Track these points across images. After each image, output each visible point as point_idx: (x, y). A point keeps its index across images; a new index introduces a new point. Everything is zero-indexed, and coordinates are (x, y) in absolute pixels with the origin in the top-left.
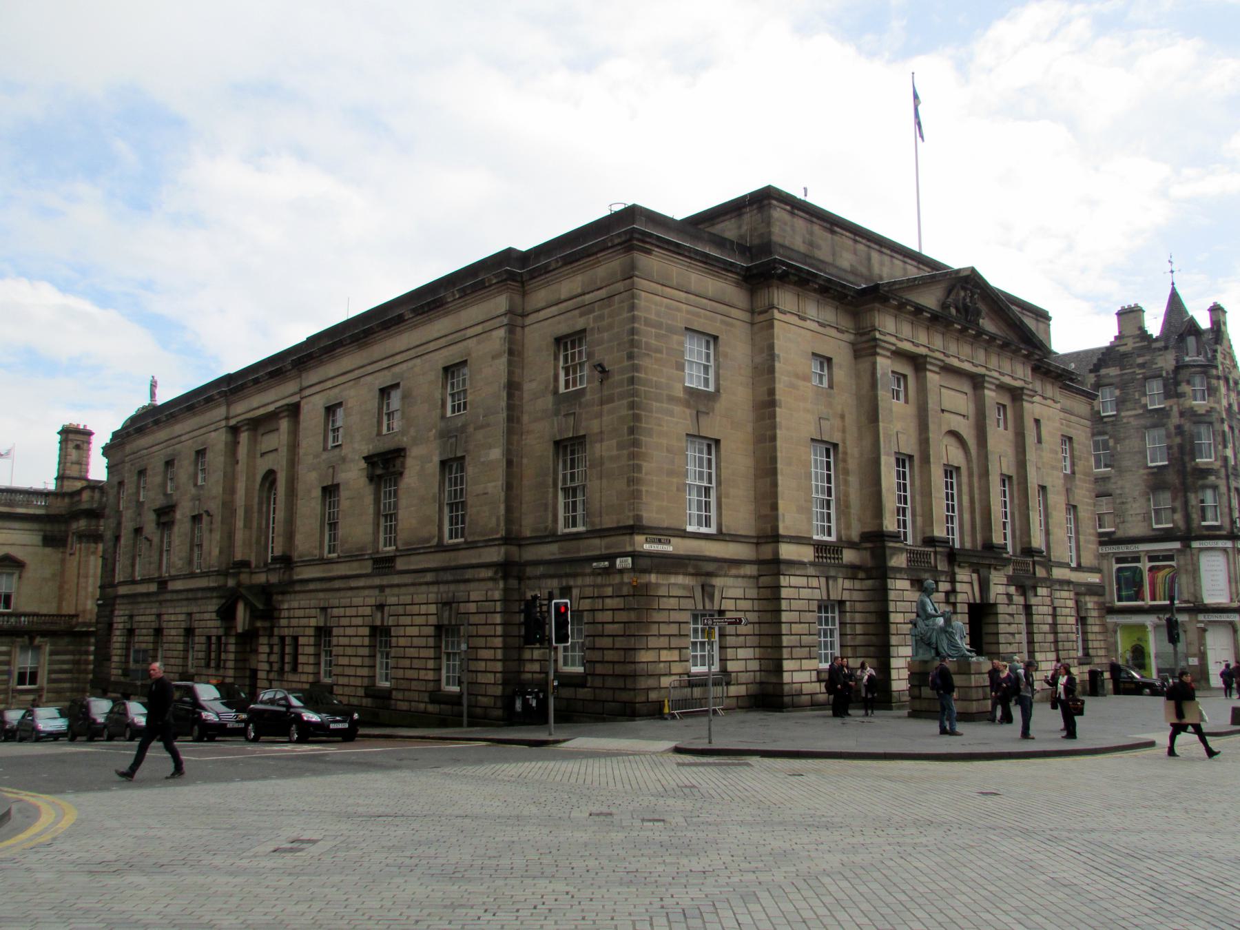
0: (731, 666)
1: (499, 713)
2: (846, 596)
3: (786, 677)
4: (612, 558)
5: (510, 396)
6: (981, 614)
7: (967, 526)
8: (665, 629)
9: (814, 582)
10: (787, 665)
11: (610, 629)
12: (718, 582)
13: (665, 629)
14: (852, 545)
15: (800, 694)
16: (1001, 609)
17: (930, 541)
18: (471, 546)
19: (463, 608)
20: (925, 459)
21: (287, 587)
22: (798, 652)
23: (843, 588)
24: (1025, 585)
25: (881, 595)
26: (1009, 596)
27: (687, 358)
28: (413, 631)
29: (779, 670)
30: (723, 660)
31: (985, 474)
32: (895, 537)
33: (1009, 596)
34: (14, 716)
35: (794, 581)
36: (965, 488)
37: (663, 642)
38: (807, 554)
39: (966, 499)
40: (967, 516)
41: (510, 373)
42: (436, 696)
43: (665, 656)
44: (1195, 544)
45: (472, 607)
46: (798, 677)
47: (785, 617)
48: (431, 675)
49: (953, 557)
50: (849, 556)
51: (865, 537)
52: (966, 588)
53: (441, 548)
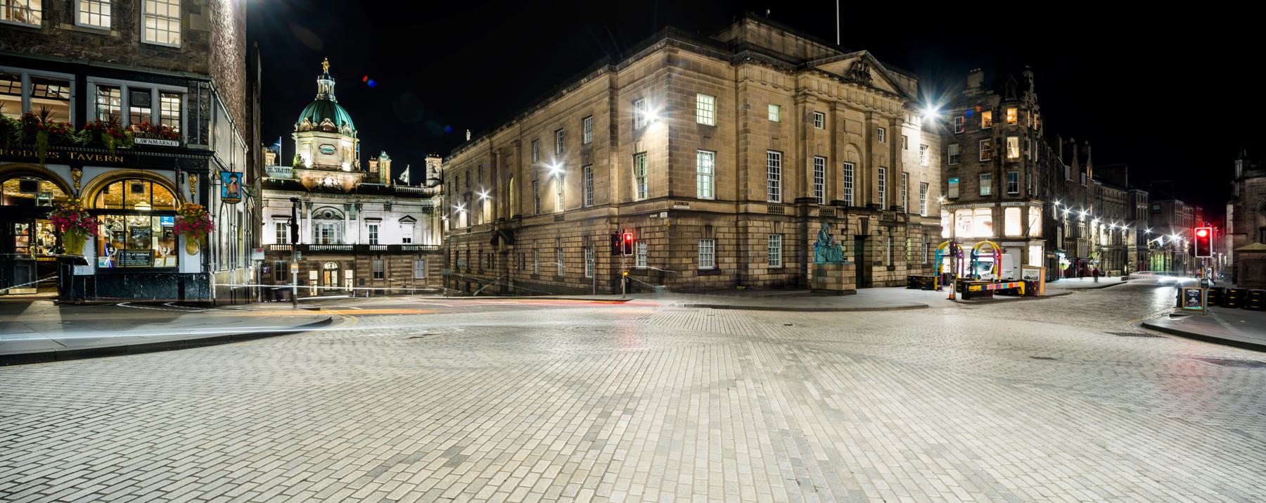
0: (721, 266)
1: (609, 288)
2: (786, 231)
3: (750, 272)
4: (658, 213)
5: (612, 132)
6: (861, 239)
7: (859, 195)
8: (685, 248)
9: (768, 224)
10: (750, 266)
11: (658, 248)
12: (715, 223)
13: (685, 248)
14: (789, 205)
15: (758, 280)
16: (874, 238)
17: (834, 203)
18: (596, 207)
19: (593, 238)
20: (834, 159)
21: (520, 229)
22: (757, 259)
23: (785, 227)
24: (890, 224)
25: (805, 230)
26: (880, 232)
27: (434, 164)
28: (572, 250)
29: (746, 268)
30: (717, 263)
31: (870, 166)
32: (813, 200)
33: (880, 232)
34: (12, 188)
35: (756, 223)
36: (858, 175)
37: (684, 254)
38: (763, 209)
39: (858, 181)
40: (859, 190)
41: (612, 121)
42: (583, 279)
43: (684, 261)
44: (1003, 204)
45: (597, 238)
46: (756, 272)
47: (750, 242)
48: (580, 271)
49: (847, 209)
50: (788, 210)
51: (797, 200)
52: (854, 227)
53: (583, 208)
